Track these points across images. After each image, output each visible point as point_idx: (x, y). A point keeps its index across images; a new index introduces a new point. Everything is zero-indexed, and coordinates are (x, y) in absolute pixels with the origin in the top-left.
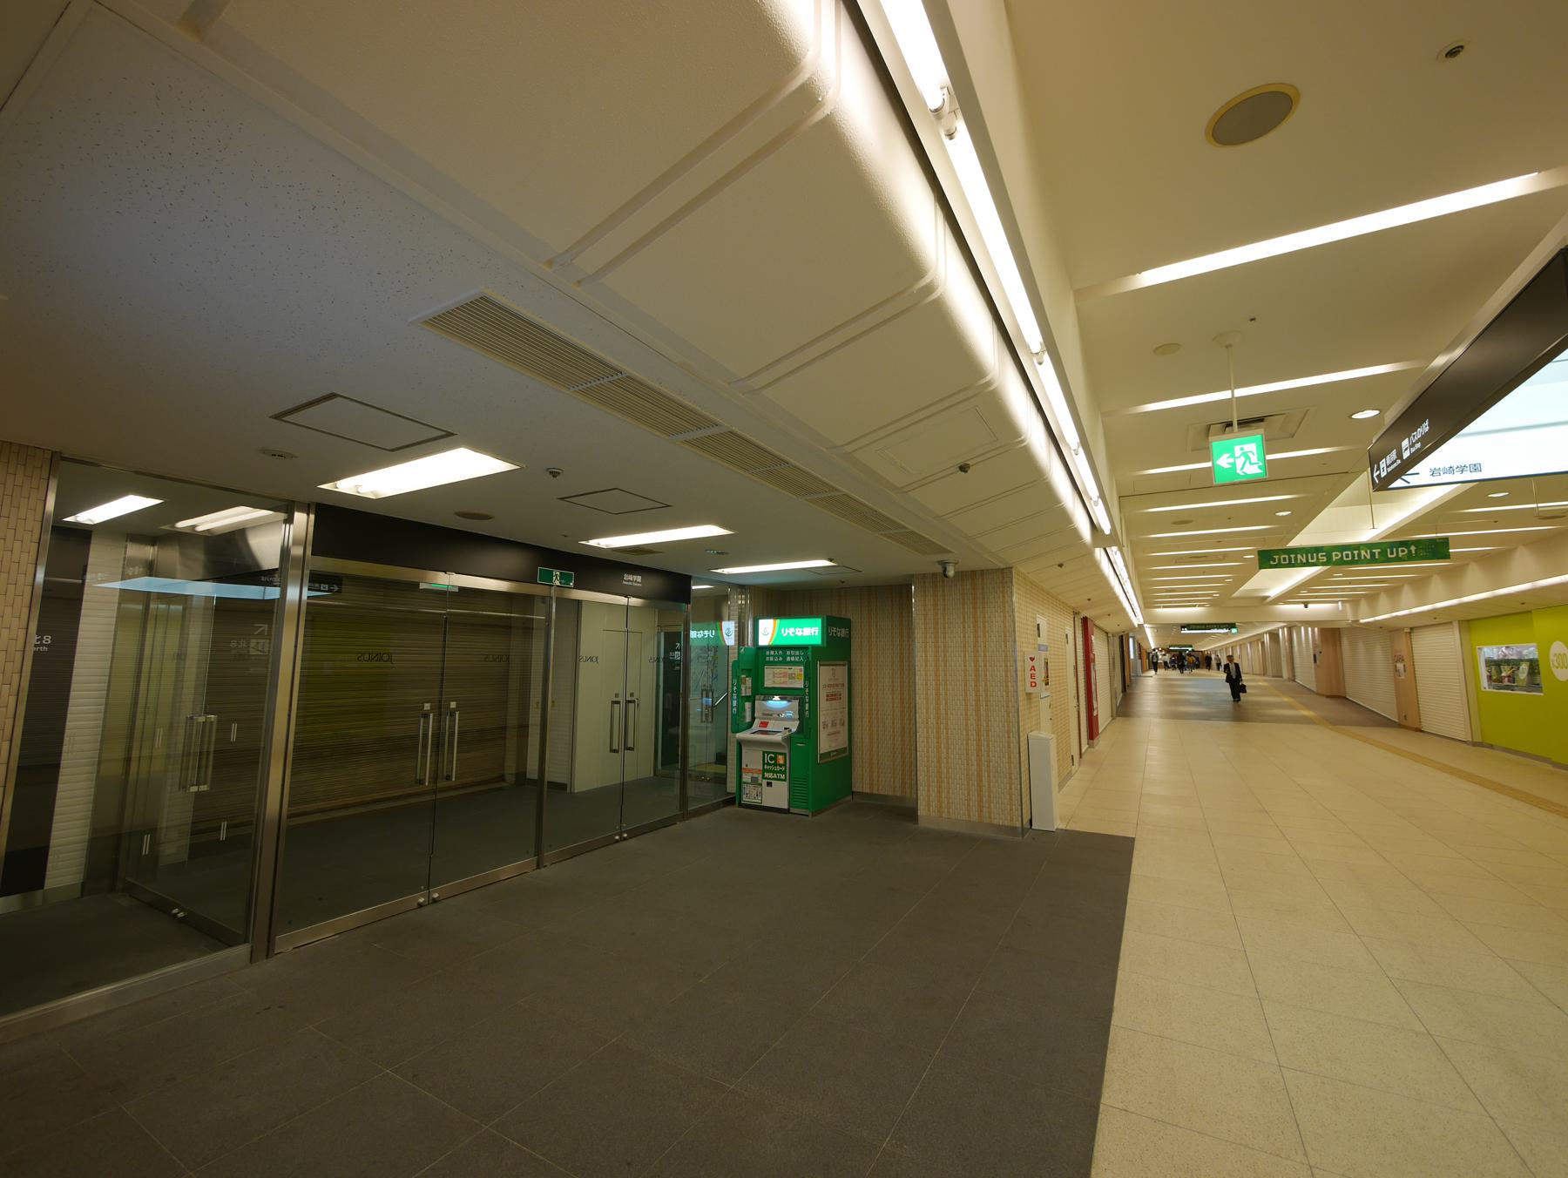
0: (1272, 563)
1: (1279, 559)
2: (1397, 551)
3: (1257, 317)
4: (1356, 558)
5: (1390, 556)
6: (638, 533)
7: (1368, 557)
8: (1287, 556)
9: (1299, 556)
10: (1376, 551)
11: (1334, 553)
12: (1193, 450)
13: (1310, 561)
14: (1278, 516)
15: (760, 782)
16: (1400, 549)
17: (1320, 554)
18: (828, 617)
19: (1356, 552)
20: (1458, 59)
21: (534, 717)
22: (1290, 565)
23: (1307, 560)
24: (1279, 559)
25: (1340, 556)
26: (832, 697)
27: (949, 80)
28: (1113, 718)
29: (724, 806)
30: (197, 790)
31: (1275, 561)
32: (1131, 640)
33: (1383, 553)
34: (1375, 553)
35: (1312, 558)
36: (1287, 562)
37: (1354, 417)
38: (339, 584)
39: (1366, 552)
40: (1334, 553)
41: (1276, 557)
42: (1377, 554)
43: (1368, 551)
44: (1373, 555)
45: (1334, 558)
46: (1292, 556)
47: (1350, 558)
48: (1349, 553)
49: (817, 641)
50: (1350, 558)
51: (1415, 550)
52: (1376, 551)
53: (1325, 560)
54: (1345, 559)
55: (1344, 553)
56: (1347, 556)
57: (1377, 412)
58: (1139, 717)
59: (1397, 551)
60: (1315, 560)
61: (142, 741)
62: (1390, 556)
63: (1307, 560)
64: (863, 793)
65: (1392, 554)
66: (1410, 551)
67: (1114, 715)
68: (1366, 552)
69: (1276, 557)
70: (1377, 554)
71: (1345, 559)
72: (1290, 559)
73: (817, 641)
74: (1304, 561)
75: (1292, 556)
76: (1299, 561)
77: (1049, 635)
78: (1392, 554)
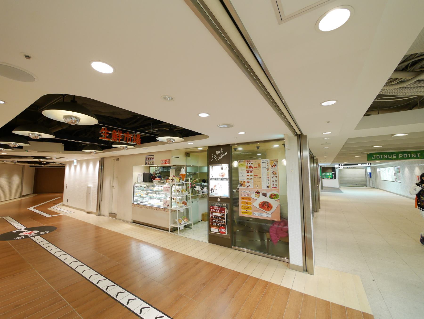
0: (373, 158)
1: (376, 157)
2: (392, 156)
3: (67, 199)
4: (409, 157)
8: (379, 156)
9: (384, 156)
11: (399, 155)
13: (389, 158)
14: (260, 154)
17: (393, 155)
19: (409, 154)
20: (69, 200)
21: (37, 160)
22: (380, 159)
23: (388, 157)
24: (376, 157)
25: (402, 156)
31: (374, 158)
34: (374, 156)
35: (390, 156)
36: (407, 157)
40: (399, 155)
41: (375, 156)
43: (415, 154)
44: (417, 156)
45: (400, 157)
48: (406, 155)
52: (419, 154)
53: (396, 157)
54: (404, 157)
55: (404, 155)
59: (392, 156)
63: (388, 157)
64: (86, 197)
68: (414, 155)
69: (375, 156)
71: (404, 157)
72: (408, 156)
74: (387, 157)
76: (412, 157)
77: (233, 201)
78: (394, 156)
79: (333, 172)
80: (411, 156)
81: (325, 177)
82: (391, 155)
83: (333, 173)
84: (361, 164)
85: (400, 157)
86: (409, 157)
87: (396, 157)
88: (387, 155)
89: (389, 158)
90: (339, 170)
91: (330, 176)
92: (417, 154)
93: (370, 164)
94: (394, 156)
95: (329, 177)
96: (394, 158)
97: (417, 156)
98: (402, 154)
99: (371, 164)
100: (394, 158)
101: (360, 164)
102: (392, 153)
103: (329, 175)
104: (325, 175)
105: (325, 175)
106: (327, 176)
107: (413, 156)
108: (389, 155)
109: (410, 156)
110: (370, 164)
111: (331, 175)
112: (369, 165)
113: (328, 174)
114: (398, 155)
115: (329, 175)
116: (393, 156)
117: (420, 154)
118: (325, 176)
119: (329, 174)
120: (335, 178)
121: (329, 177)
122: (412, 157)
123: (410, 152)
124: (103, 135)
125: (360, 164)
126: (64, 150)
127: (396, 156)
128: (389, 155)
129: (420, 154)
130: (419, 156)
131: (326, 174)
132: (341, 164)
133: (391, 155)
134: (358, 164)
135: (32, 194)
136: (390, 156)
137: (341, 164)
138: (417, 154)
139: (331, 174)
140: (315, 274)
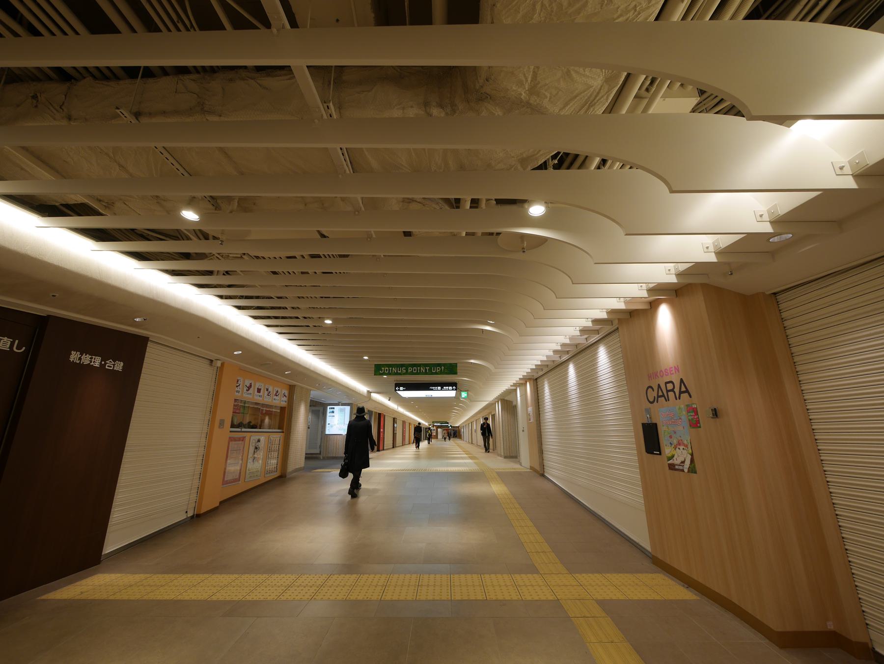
0: (380, 372)
1: (384, 370)
7: (424, 371)
13: (398, 372)
18: (285, 407)
24: (384, 370)
26: (178, 22)
27: (148, 349)
28: (484, 98)
29: (279, 317)
32: (450, 393)
33: (430, 370)
41: (383, 368)
46: (391, 368)
49: (329, 431)
58: (683, 88)
60: (112, 366)
63: (397, 371)
65: (434, 370)
67: (854, 174)
69: (383, 368)
73: (329, 431)
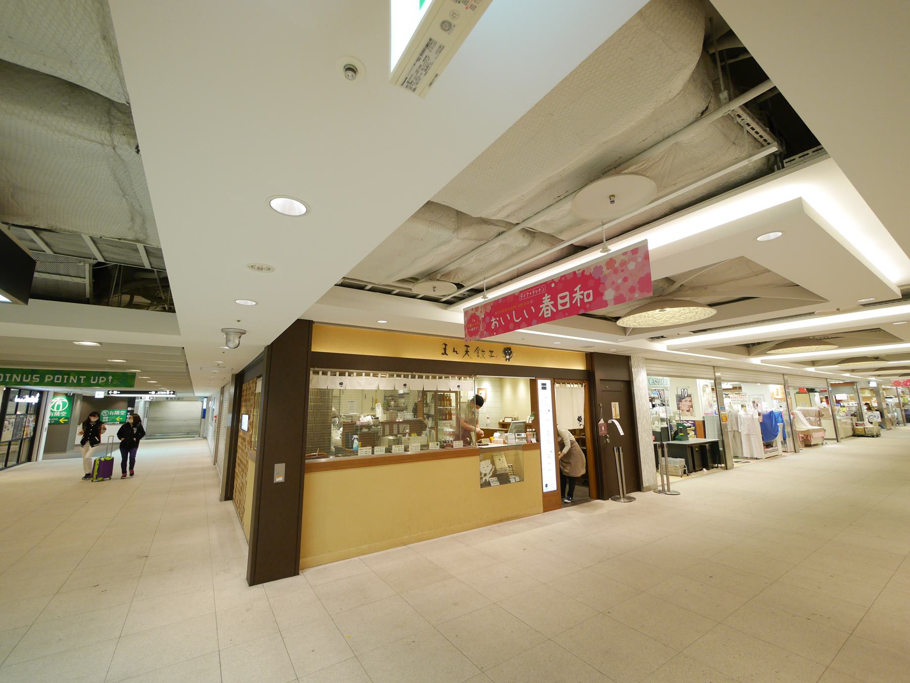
2: (32, 377)
4: (65, 382)
5: (92, 382)
6: (868, 319)
10: (110, 378)
11: (47, 376)
12: (606, 241)
15: (582, 434)
16: (101, 378)
17: (34, 376)
23: (22, 379)
25: (52, 378)
30: (376, 448)
35: (27, 378)
37: (758, 239)
38: (101, 272)
39: (75, 378)
42: (82, 380)
43: (76, 377)
44: (79, 380)
45: (47, 380)
46: (8, 375)
47: (60, 381)
48: (61, 377)
50: (60, 381)
51: (112, 379)
52: (83, 377)
53: (38, 381)
55: (56, 376)
56: (58, 379)
57: (780, 234)
59: (32, 377)
61: (107, 448)
62: (92, 382)
63: (22, 379)
65: (94, 380)
66: (108, 380)
68: (75, 378)
70: (82, 380)
72: (63, 380)
75: (66, 377)
78: (94, 380)
79: (130, 409)
80: (69, 380)
81: (107, 420)
82: (30, 376)
83: (128, 411)
84: (156, 392)
85: (46, 381)
86: (65, 382)
87: (40, 381)
88: (20, 375)
89: (24, 380)
90: (147, 405)
91: (121, 416)
92: (80, 377)
93: (172, 392)
94: (36, 377)
95: (117, 419)
96: (34, 381)
97: (79, 380)
98: (52, 375)
99: (174, 392)
100: (34, 381)
101: (154, 393)
102: (33, 372)
103: (119, 415)
104: (109, 416)
105: (109, 416)
106: (114, 417)
107: (75, 379)
108: (25, 375)
109: (9, 379)
110: (172, 392)
111: (123, 414)
112: (170, 394)
113: (117, 412)
114: (45, 377)
115: (117, 416)
116: (34, 378)
117: (85, 377)
118: (107, 418)
119: (118, 411)
120: (740, 388)
121: (117, 419)
122: (70, 382)
123: (68, 373)
124: (719, 50)
125: (154, 393)
126: (242, 568)
127: (38, 379)
128: (25, 375)
129: (85, 377)
130: (82, 382)
131: (111, 413)
132: (113, 391)
133: (30, 376)
134: (150, 393)
135: (850, 436)
136: (27, 378)
137: (113, 391)
138: (80, 377)
139: (123, 412)
140: (259, 589)
